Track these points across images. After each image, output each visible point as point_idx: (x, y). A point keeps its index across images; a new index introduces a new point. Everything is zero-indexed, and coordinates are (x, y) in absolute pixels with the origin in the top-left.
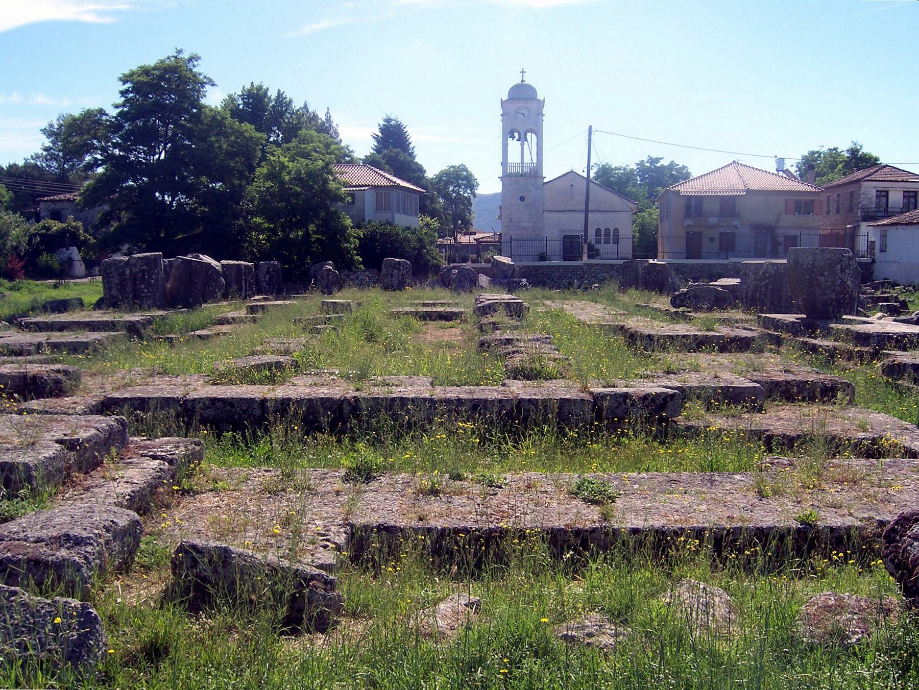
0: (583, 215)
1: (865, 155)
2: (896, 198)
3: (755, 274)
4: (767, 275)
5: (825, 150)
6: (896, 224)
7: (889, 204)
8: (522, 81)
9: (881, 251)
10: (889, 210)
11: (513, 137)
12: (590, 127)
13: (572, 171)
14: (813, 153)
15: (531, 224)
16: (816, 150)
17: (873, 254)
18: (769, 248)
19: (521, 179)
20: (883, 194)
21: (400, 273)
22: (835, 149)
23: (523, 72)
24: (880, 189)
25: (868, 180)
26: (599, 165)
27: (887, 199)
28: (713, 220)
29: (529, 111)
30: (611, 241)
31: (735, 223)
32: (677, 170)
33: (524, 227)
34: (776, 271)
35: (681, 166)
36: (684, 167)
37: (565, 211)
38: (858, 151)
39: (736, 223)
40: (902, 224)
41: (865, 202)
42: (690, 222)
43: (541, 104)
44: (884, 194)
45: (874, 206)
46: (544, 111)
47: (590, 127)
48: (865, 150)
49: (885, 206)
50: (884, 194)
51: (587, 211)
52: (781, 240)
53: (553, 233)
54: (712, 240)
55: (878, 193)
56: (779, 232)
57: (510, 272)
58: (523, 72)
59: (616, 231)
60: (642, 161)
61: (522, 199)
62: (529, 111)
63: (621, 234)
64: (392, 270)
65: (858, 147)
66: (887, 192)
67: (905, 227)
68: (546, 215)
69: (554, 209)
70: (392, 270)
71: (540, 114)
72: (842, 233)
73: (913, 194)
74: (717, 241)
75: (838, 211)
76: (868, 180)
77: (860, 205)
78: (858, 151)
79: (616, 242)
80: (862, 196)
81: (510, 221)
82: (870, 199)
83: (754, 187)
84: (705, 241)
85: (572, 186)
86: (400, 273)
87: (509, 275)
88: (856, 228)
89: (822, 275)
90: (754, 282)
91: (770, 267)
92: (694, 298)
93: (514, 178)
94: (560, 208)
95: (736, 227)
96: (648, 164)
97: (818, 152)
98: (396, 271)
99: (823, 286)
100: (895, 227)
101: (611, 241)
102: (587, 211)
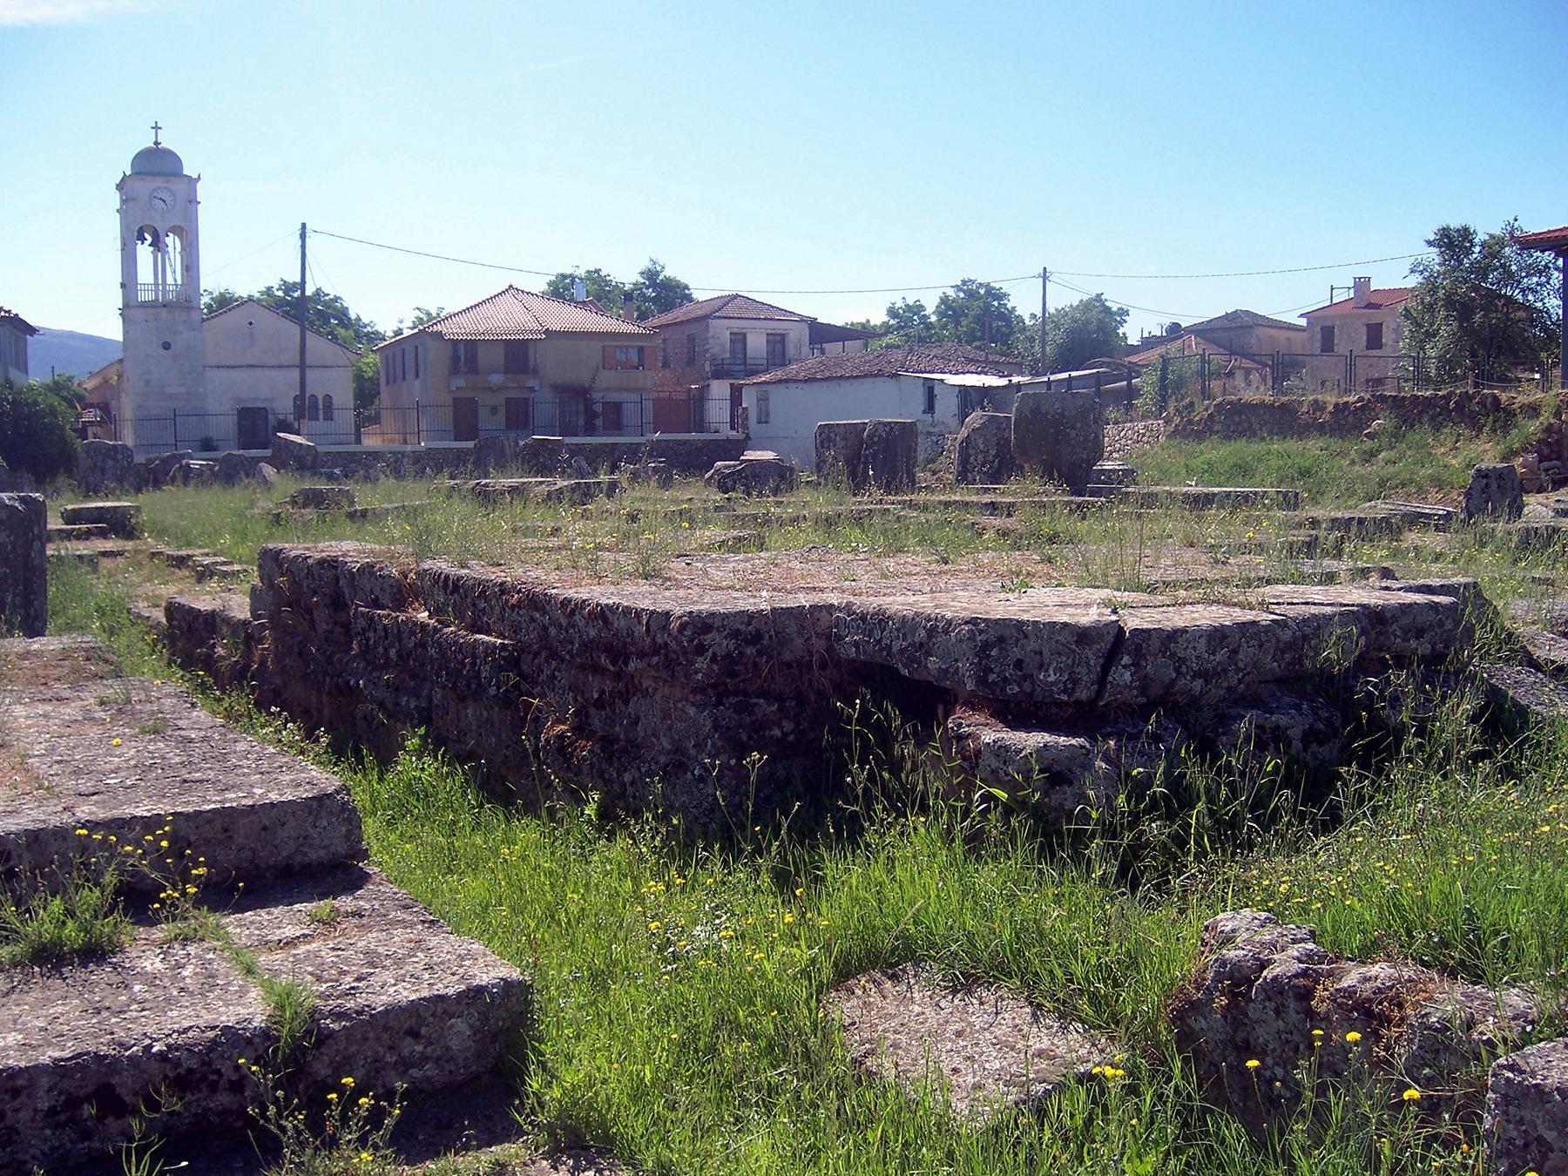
0: (296, 373)
1: (668, 279)
2: (757, 344)
3: (845, 439)
4: (876, 439)
5: (581, 272)
6: (780, 381)
7: (748, 353)
8: (156, 143)
9: (759, 422)
10: (749, 361)
11: (143, 240)
12: (304, 226)
13: (511, 286)
14: (564, 277)
15: (183, 390)
16: (568, 271)
17: (746, 427)
18: (582, 422)
19: (163, 312)
20: (739, 339)
21: (118, 466)
22: (598, 271)
23: (156, 128)
24: (735, 330)
25: (719, 317)
26: (211, 293)
27: (745, 345)
28: (497, 379)
29: (174, 195)
30: (321, 417)
31: (529, 384)
32: (325, 304)
33: (171, 395)
34: (888, 434)
35: (332, 297)
36: (337, 299)
37: (240, 367)
38: (657, 273)
39: (532, 382)
40: (795, 381)
41: (716, 350)
42: (460, 382)
43: (193, 182)
44: (740, 337)
45: (728, 355)
46: (201, 195)
47: (304, 226)
48: (668, 273)
49: (741, 356)
50: (779, 338)
51: (303, 367)
52: (599, 408)
53: (221, 404)
54: (494, 410)
55: (733, 337)
56: (597, 396)
57: (309, 458)
58: (156, 128)
59: (328, 398)
60: (270, 288)
61: (167, 346)
62: (174, 196)
63: (337, 402)
64: (104, 461)
65: (659, 269)
66: (744, 335)
67: (800, 385)
68: (209, 373)
69: (224, 363)
70: (104, 461)
71: (193, 201)
72: (682, 397)
73: (779, 338)
74: (502, 411)
75: (666, 365)
76: (719, 317)
77: (708, 355)
78: (657, 273)
79: (329, 417)
80: (711, 341)
81: (148, 383)
82: (722, 345)
83: (555, 326)
84: (483, 413)
85: (251, 323)
86: (118, 466)
87: (309, 463)
88: (704, 389)
89: (1073, 428)
90: (843, 451)
91: (881, 428)
92: (753, 477)
93: (151, 311)
94: (232, 363)
95: (532, 389)
96: (280, 293)
97: (571, 275)
98: (110, 462)
99: (1073, 442)
100: (785, 385)
101: (321, 417)
102: (303, 367)
